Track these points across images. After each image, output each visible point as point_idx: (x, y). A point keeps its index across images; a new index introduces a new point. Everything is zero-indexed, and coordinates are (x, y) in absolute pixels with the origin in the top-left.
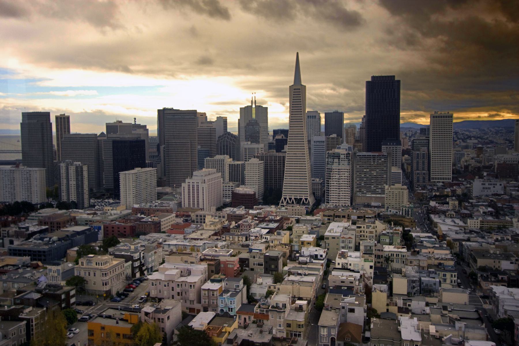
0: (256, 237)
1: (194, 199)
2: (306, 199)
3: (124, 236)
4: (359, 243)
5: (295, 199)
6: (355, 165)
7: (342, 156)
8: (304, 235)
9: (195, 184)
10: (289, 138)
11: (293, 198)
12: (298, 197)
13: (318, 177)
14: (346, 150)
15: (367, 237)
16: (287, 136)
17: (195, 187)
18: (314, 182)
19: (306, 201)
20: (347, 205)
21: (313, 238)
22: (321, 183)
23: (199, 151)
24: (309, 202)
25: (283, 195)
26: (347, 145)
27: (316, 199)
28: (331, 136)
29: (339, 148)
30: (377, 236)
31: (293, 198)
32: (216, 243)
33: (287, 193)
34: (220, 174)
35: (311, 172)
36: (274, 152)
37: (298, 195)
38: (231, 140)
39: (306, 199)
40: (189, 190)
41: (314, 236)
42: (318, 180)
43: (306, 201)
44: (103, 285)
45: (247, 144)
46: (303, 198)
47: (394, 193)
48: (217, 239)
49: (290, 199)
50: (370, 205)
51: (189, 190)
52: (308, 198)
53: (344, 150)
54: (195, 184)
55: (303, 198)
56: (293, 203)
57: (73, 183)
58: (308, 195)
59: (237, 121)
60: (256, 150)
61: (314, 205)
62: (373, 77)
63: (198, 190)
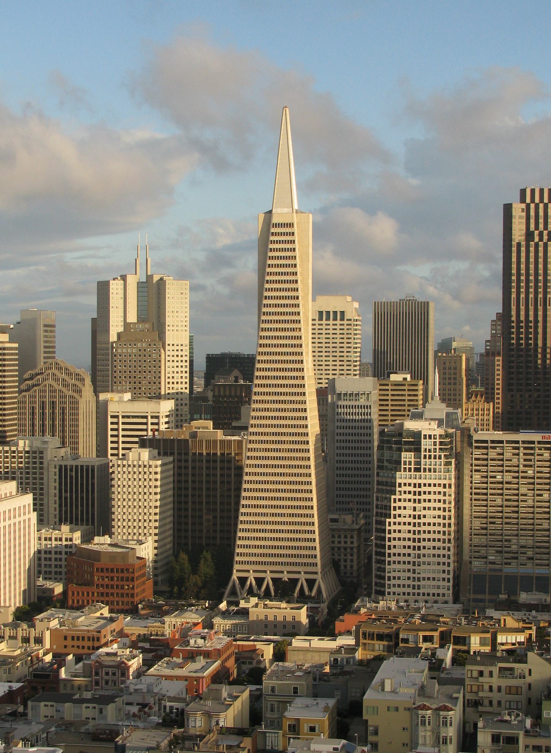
0: (144, 705)
2: (311, 583)
4: (475, 726)
5: (306, 580)
6: (467, 471)
7: (426, 444)
8: (299, 702)
10: (256, 382)
11: (268, 577)
12: (285, 577)
13: (350, 511)
15: (491, 703)
16: (249, 376)
18: (334, 526)
19: (311, 589)
21: (326, 709)
22: (359, 530)
23: (53, 590)
24: (319, 591)
25: (236, 567)
26: (444, 405)
27: (342, 583)
28: (394, 377)
29: (419, 416)
30: (533, 701)
31: (268, 577)
32: (7, 725)
33: (246, 563)
34: (28, 499)
35: (327, 496)
36: (205, 426)
37: (285, 569)
38: (66, 386)
39: (311, 583)
41: (331, 702)
42: (349, 518)
43: (311, 589)
44: (370, 406)
45: (121, 401)
46: (302, 578)
48: (14, 714)
50: (516, 602)
52: (319, 577)
53: (434, 425)
55: (302, 578)
58: (319, 569)
59: (88, 326)
60: (150, 420)
61: (333, 604)
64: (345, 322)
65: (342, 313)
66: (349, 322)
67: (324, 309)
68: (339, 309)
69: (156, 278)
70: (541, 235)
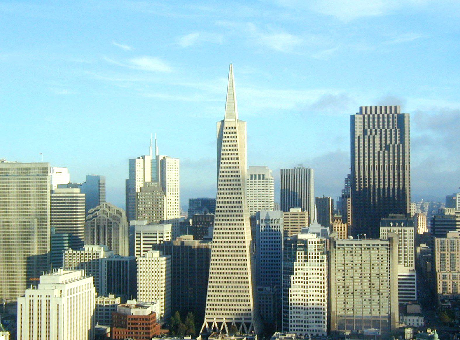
1: (39, 327)
3: (347, 338)
9: (44, 299)
10: (216, 213)
14: (318, 235)
17: (44, 304)
20: (320, 334)
25: (206, 316)
36: (188, 239)
40: (31, 309)
42: (268, 288)
47: (323, 324)
49: (219, 324)
51: (31, 309)
53: (315, 236)
54: (44, 299)
56: (224, 331)
57: (95, 237)
62: (88, 177)
63: (48, 309)
64: (265, 180)
65: (263, 175)
66: (267, 180)
67: (253, 174)
68: (261, 174)
69: (161, 158)
70: (371, 131)
